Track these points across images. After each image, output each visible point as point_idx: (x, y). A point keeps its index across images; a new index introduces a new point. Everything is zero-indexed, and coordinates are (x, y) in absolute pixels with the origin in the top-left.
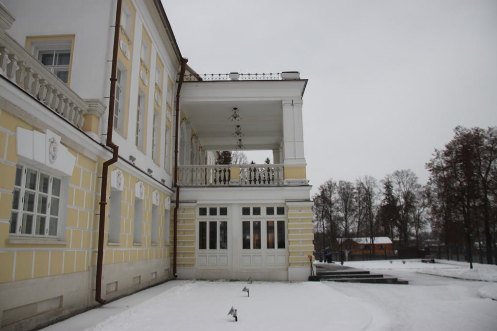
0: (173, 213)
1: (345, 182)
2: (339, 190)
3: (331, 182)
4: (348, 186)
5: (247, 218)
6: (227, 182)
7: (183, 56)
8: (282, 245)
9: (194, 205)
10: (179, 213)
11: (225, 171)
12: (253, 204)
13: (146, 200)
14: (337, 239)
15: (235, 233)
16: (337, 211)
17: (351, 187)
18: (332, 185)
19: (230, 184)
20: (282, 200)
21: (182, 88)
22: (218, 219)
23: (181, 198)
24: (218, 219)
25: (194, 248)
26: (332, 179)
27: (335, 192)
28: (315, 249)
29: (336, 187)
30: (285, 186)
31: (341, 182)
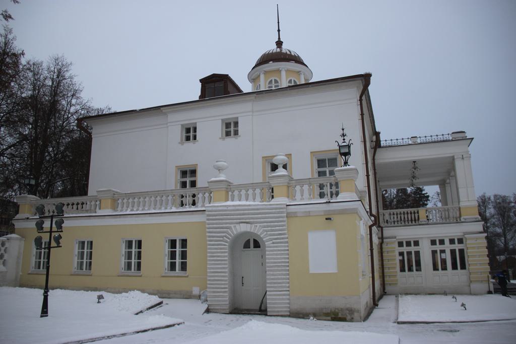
0: (379, 246)
1: (500, 196)
2: (494, 204)
3: (484, 196)
4: (504, 199)
5: (434, 248)
6: (417, 222)
7: (377, 130)
8: (463, 267)
9: (395, 239)
10: (384, 246)
11: (414, 213)
12: (406, 239)
13: (88, 198)
14: (498, 257)
15: (426, 259)
16: (493, 227)
17: (508, 201)
18: (485, 199)
19: (420, 223)
20: (461, 232)
21: (377, 152)
22: (413, 249)
23: (385, 235)
24: (413, 249)
25: (396, 272)
26: (485, 193)
27: (489, 206)
28: (491, 270)
29: (490, 202)
30: (462, 222)
31: (495, 196)
